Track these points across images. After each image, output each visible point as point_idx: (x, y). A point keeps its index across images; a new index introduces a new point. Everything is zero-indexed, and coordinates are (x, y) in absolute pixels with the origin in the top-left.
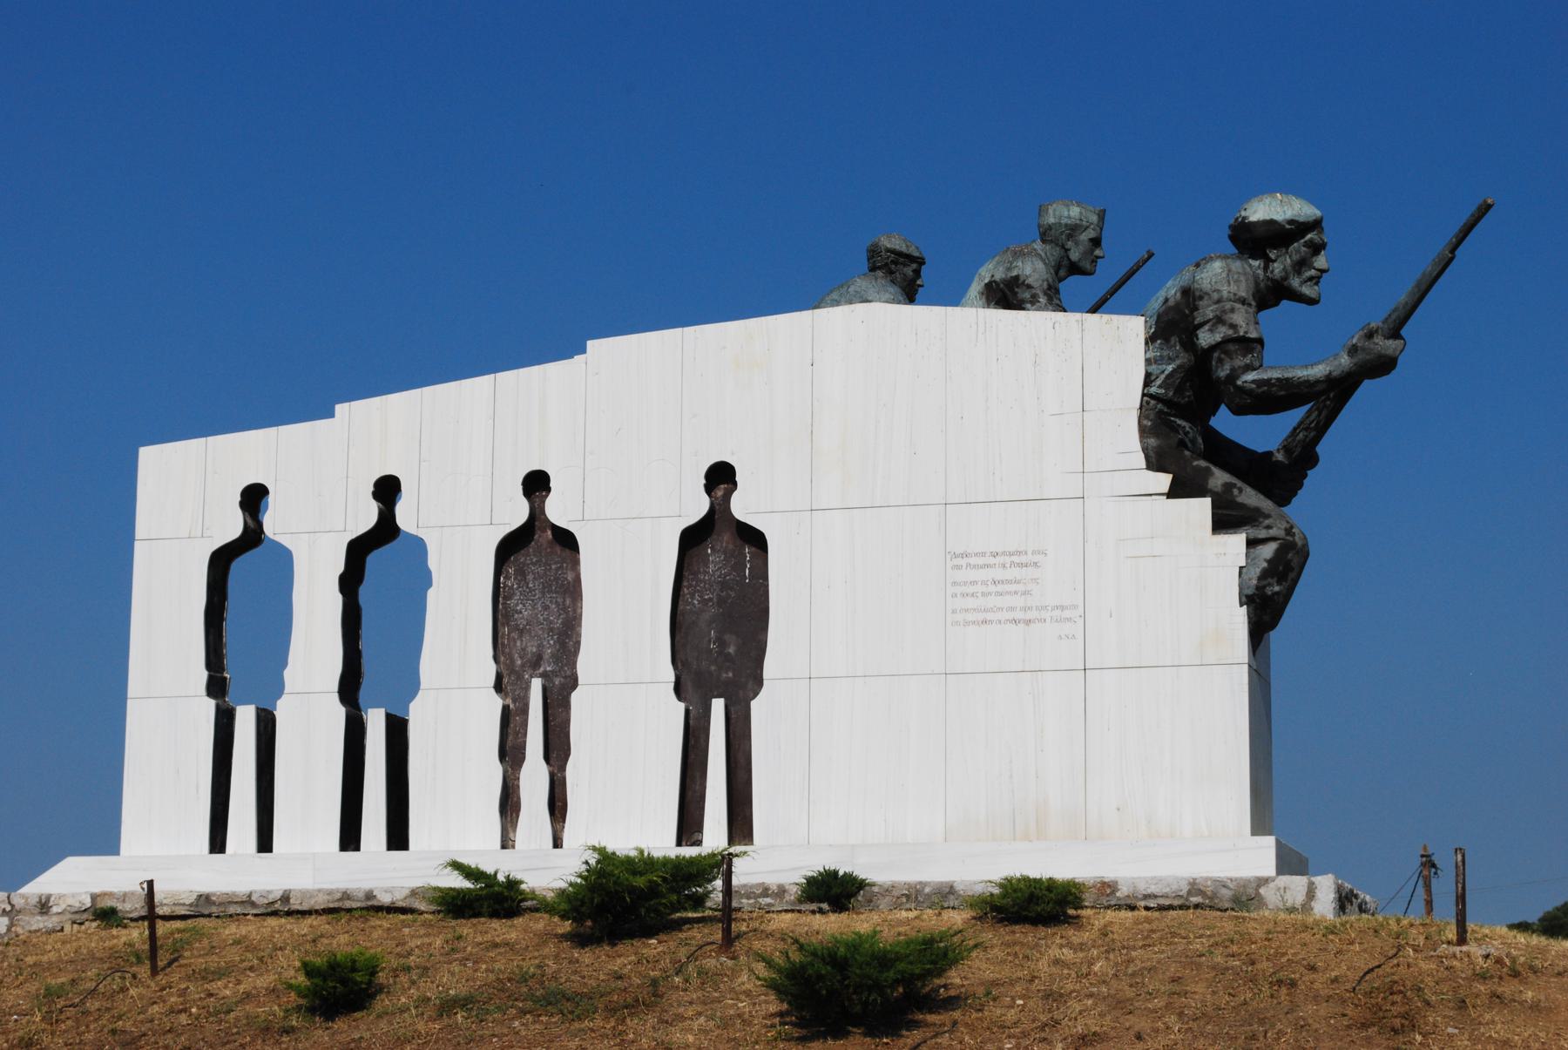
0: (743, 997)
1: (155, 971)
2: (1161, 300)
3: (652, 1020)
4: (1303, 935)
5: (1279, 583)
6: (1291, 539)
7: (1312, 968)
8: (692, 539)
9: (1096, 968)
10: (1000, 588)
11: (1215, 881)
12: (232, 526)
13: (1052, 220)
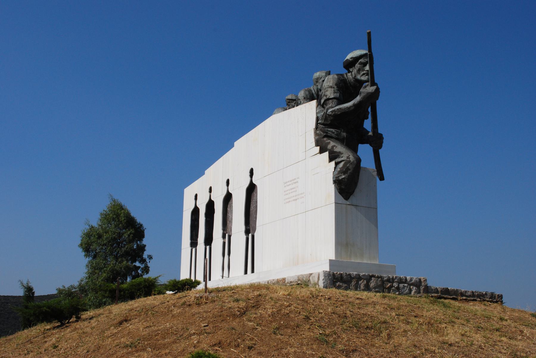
4: (90, 295)
5: (344, 174)
6: (349, 160)
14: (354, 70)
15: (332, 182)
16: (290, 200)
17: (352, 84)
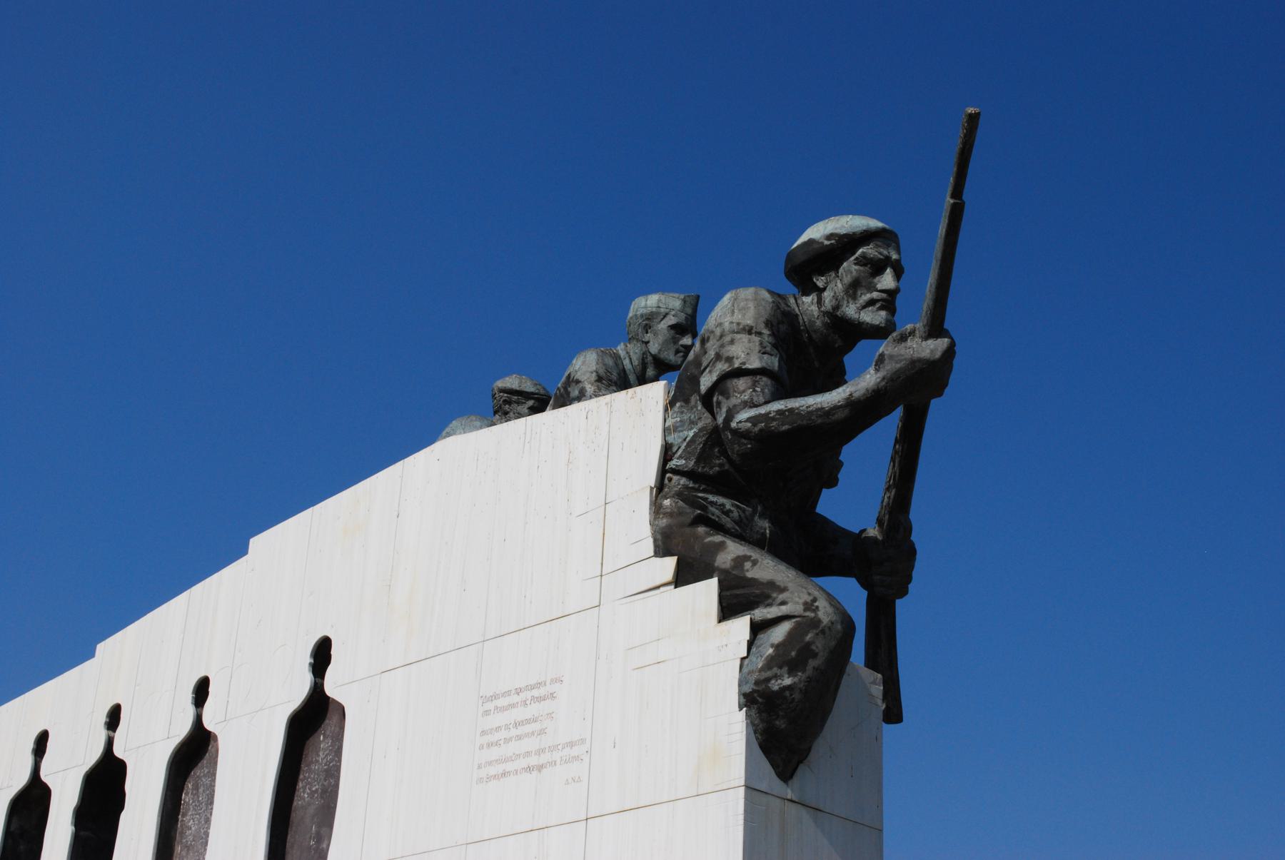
5: (791, 672)
6: (812, 615)
10: (520, 731)
14: (833, 287)
15: (733, 697)
16: (510, 767)
17: (814, 336)
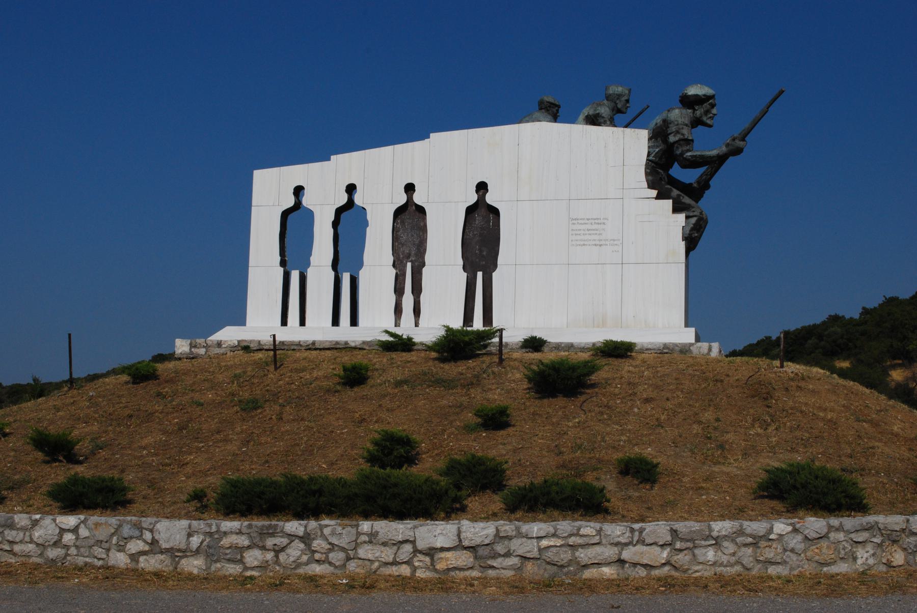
0: (512, 382)
1: (276, 369)
2: (654, 124)
3: (479, 390)
5: (697, 233)
7: (728, 376)
8: (470, 210)
9: (645, 373)
10: (590, 232)
11: (673, 344)
12: (290, 202)
13: (611, 92)
